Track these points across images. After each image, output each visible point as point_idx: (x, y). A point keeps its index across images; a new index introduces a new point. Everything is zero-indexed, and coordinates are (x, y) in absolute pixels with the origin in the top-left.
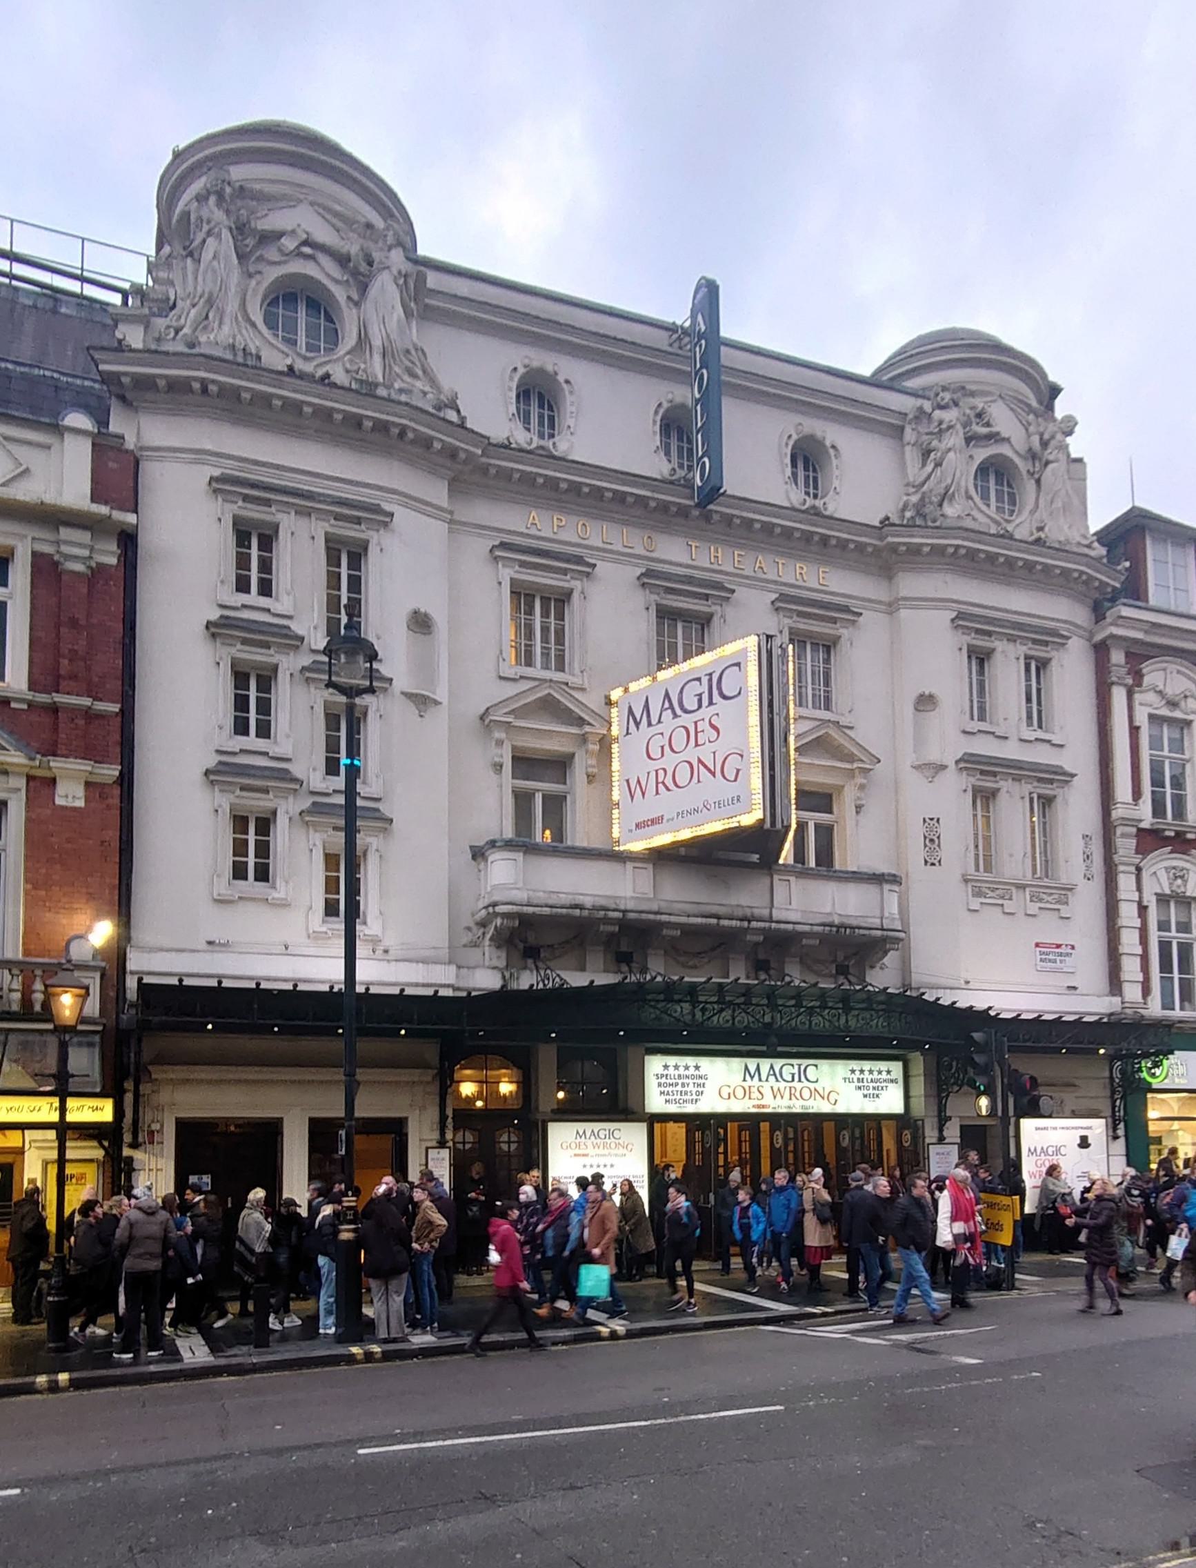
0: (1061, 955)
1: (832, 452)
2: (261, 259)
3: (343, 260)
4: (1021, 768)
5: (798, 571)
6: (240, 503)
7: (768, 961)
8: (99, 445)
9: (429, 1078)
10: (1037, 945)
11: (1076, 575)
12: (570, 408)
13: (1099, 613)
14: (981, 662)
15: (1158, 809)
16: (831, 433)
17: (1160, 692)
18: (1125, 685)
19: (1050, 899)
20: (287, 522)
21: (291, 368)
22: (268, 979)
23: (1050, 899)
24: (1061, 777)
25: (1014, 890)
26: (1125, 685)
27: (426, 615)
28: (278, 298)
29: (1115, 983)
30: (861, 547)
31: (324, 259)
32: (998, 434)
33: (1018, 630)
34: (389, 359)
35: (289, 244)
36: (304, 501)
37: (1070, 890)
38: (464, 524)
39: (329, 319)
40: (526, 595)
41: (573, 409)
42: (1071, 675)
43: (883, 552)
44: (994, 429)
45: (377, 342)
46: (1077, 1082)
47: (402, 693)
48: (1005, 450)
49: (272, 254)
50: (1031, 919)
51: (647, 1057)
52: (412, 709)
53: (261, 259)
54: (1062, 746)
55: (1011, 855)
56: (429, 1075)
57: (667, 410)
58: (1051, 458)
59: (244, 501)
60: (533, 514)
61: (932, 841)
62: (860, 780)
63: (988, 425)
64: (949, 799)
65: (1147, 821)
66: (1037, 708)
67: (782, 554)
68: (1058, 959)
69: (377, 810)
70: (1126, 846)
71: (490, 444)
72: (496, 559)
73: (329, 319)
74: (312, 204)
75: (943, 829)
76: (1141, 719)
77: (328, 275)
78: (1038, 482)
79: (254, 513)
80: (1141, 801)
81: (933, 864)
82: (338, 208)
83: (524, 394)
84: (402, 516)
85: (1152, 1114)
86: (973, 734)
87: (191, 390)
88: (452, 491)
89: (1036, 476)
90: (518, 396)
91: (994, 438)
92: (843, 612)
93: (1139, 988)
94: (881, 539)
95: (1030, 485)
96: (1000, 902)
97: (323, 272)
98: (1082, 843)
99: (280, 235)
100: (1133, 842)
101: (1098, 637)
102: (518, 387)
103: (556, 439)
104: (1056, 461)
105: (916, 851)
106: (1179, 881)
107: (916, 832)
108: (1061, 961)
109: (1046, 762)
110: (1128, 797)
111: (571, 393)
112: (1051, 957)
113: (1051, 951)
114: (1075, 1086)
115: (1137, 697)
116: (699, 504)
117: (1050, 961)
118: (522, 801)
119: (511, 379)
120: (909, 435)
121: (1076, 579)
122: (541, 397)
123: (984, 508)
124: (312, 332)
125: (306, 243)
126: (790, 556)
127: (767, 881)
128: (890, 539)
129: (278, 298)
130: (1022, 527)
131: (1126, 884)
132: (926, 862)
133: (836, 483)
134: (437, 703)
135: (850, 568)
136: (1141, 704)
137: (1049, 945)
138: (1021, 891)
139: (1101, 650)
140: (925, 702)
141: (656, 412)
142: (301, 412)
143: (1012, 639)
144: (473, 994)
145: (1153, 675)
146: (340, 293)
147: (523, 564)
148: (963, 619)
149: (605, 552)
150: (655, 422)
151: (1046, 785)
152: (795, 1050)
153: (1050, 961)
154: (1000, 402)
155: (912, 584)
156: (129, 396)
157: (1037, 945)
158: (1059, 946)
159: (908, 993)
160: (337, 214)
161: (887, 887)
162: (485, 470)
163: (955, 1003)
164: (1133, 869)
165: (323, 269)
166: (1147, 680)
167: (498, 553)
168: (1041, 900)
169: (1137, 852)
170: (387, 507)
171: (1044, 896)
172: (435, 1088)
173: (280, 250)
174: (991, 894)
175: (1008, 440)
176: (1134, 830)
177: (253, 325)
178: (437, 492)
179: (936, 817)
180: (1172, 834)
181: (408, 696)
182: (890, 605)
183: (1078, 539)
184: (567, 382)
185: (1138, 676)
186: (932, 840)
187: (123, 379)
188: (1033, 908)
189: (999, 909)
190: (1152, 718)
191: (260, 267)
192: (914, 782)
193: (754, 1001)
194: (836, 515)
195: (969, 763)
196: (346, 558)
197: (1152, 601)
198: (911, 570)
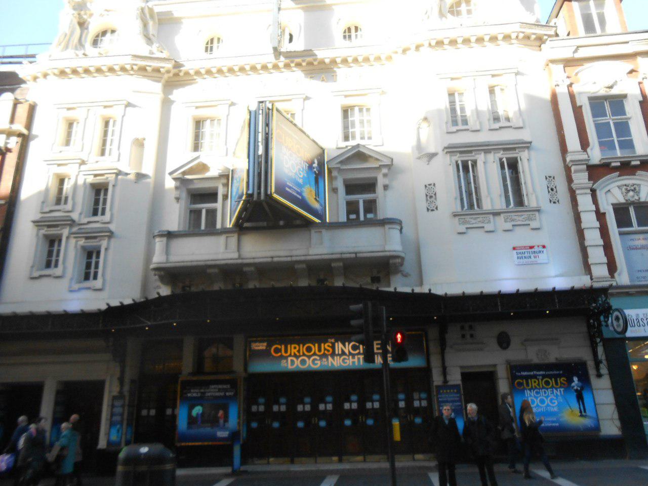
15: (606, 145)
19: (521, 218)
20: (481, 158)
25: (491, 217)
29: (587, 268)
59: (460, 154)
61: (431, 197)
65: (596, 155)
70: (581, 178)
81: (432, 210)
85: (228, 227)
93: (605, 268)
106: (631, 193)
108: (535, 257)
109: (589, 136)
112: (526, 255)
113: (527, 252)
117: (525, 257)
118: (196, 214)
131: (585, 202)
132: (428, 209)
137: (525, 248)
153: (525, 257)
157: (514, 249)
158: (531, 247)
161: (387, 227)
164: (589, 191)
168: (513, 220)
169: (590, 179)
171: (515, 217)
174: (473, 221)
176: (585, 167)
180: (638, 163)
187: (147, 68)
188: (508, 226)
195: (451, 150)
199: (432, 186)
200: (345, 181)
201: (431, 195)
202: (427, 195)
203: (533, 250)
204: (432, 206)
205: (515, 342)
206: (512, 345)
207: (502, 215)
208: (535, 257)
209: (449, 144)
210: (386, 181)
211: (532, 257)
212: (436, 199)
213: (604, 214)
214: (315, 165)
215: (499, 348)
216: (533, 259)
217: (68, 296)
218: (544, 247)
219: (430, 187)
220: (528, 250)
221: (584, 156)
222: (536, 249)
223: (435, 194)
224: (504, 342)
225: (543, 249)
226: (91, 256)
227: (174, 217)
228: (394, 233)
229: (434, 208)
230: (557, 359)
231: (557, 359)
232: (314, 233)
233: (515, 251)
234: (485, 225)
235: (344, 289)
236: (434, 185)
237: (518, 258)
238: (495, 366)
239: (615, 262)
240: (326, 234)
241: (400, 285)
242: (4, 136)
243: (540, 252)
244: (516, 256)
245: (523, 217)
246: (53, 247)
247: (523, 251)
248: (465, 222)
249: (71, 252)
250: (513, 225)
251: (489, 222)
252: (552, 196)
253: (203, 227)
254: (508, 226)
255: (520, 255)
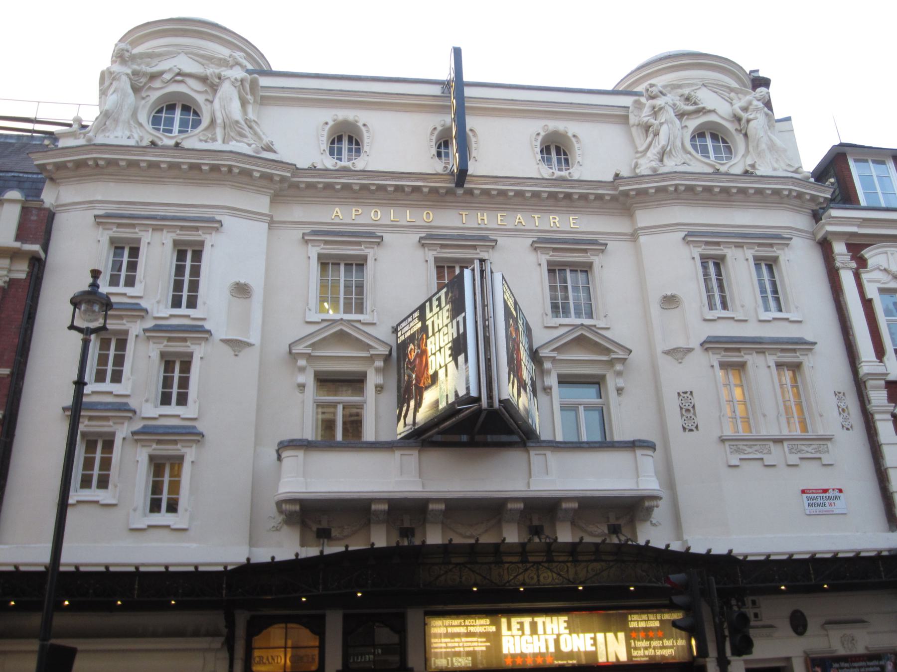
0: (829, 498)
1: (574, 140)
2: (150, 88)
3: (203, 79)
4: (760, 343)
5: (552, 221)
6: (115, 229)
7: (542, 527)
8: (27, 208)
9: (219, 645)
10: (803, 492)
11: (786, 193)
12: (578, 152)
13: (817, 217)
14: (770, 268)
16: (570, 128)
17: (885, 270)
18: (851, 269)
19: (809, 449)
21: (177, 145)
22: (144, 565)
23: (809, 449)
24: (804, 345)
25: (771, 444)
26: (851, 269)
27: (245, 285)
28: (162, 108)
30: (599, 197)
31: (191, 82)
32: (704, 108)
33: (742, 238)
34: (228, 129)
35: (167, 76)
36: (158, 222)
37: (830, 439)
38: (284, 222)
39: (724, 141)
40: (448, 267)
41: (321, 139)
42: (800, 266)
43: (622, 198)
44: (701, 106)
45: (219, 121)
46: (865, 618)
47: (221, 340)
48: (712, 118)
49: (157, 84)
50: (794, 469)
51: (427, 620)
52: (227, 350)
53: (150, 88)
54: (800, 322)
55: (764, 416)
56: (218, 643)
57: (441, 131)
58: (751, 117)
60: (519, 216)
61: (688, 410)
62: (618, 367)
63: (695, 103)
64: (700, 374)
66: (774, 294)
67: (463, 208)
68: (827, 502)
69: (194, 427)
71: (297, 169)
72: (307, 242)
73: (724, 141)
74: (186, 54)
75: (696, 400)
76: (872, 292)
77: (192, 89)
78: (746, 135)
79: (125, 233)
80: (885, 359)
81: (691, 430)
82: (202, 52)
83: (546, 150)
84: (228, 221)
86: (769, 321)
87: (88, 166)
88: (272, 202)
89: (743, 132)
90: (542, 151)
91: (702, 111)
92: (596, 245)
94: (616, 189)
95: (739, 139)
96: (759, 456)
97: (192, 89)
98: (834, 400)
99: (161, 73)
100: (884, 394)
101: (820, 236)
102: (541, 145)
103: (571, 171)
104: (756, 119)
105: (674, 420)
107: (672, 405)
110: (873, 357)
111: (368, 131)
112: (819, 501)
114: (863, 622)
115: (865, 277)
116: (459, 186)
117: (819, 505)
119: (536, 140)
120: (633, 119)
121: (788, 196)
122: (350, 139)
123: (707, 160)
124: (716, 150)
125: (179, 74)
126: (472, 208)
127: (525, 455)
128: (621, 188)
129: (162, 108)
130: (736, 165)
132: (684, 429)
133: (579, 159)
134: (249, 345)
135: (593, 213)
136: (869, 281)
137: (816, 491)
138: (779, 446)
139: (825, 246)
140: (670, 301)
141: (432, 134)
142: (201, 169)
143: (739, 246)
144: (229, 568)
145: (875, 257)
146: (200, 99)
147: (326, 242)
148: (691, 236)
149: (394, 227)
150: (431, 140)
151: (791, 356)
152: (615, 604)
153: (819, 505)
154: (704, 89)
155: (645, 218)
156: (54, 176)
157: (803, 492)
158: (825, 491)
159: (630, 543)
160: (202, 56)
161: (639, 452)
162: (296, 186)
163: (710, 551)
164: (889, 417)
165: (189, 87)
166: (871, 262)
167: (306, 238)
170: (218, 218)
171: (803, 448)
172: (227, 655)
173: (163, 82)
174: (749, 450)
175: (714, 111)
176: (883, 382)
177: (141, 125)
178: (261, 203)
179: (688, 390)
181: (226, 341)
182: (632, 235)
183: (785, 167)
184: (364, 125)
185: (862, 263)
186: (688, 410)
188: (793, 459)
189: (759, 463)
190: (882, 291)
191: (148, 93)
192: (666, 365)
193: (531, 559)
194: (582, 178)
195: (710, 344)
196: (189, 256)
197: (863, 202)
198: (645, 208)
199: (688, 395)
200: (559, 376)
201: (687, 407)
202: (681, 408)
203: (827, 495)
204: (689, 425)
205: (813, 626)
206: (809, 632)
207: (785, 444)
208: (830, 505)
209: (708, 337)
210: (620, 383)
211: (827, 505)
212: (695, 414)
213: (870, 301)
214: (40, 160)
215: (794, 634)
216: (828, 507)
217: (114, 537)
218: (840, 491)
219: (685, 396)
220: (821, 495)
221: (880, 369)
222: (831, 494)
223: (694, 407)
224: (799, 624)
225: (841, 494)
226: (164, 468)
227: (301, 415)
228: (647, 462)
229: (693, 428)
230: (867, 648)
231: (867, 648)
232: (536, 457)
233: (805, 496)
234: (765, 457)
235: (446, 549)
236: (691, 393)
237: (809, 505)
238: (788, 659)
239: (729, 559)
240: (553, 459)
241: (655, 534)
242: (6, 262)
243: (836, 498)
244: (806, 503)
245: (812, 447)
246: (94, 452)
247: (815, 495)
248: (738, 451)
249: (132, 466)
250: (801, 459)
251: (769, 452)
252: (845, 419)
253: (339, 436)
254: (793, 459)
255: (811, 502)
